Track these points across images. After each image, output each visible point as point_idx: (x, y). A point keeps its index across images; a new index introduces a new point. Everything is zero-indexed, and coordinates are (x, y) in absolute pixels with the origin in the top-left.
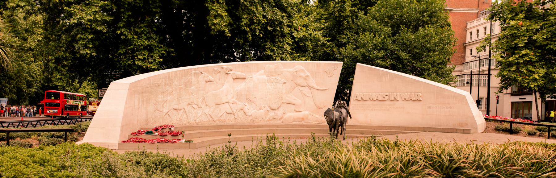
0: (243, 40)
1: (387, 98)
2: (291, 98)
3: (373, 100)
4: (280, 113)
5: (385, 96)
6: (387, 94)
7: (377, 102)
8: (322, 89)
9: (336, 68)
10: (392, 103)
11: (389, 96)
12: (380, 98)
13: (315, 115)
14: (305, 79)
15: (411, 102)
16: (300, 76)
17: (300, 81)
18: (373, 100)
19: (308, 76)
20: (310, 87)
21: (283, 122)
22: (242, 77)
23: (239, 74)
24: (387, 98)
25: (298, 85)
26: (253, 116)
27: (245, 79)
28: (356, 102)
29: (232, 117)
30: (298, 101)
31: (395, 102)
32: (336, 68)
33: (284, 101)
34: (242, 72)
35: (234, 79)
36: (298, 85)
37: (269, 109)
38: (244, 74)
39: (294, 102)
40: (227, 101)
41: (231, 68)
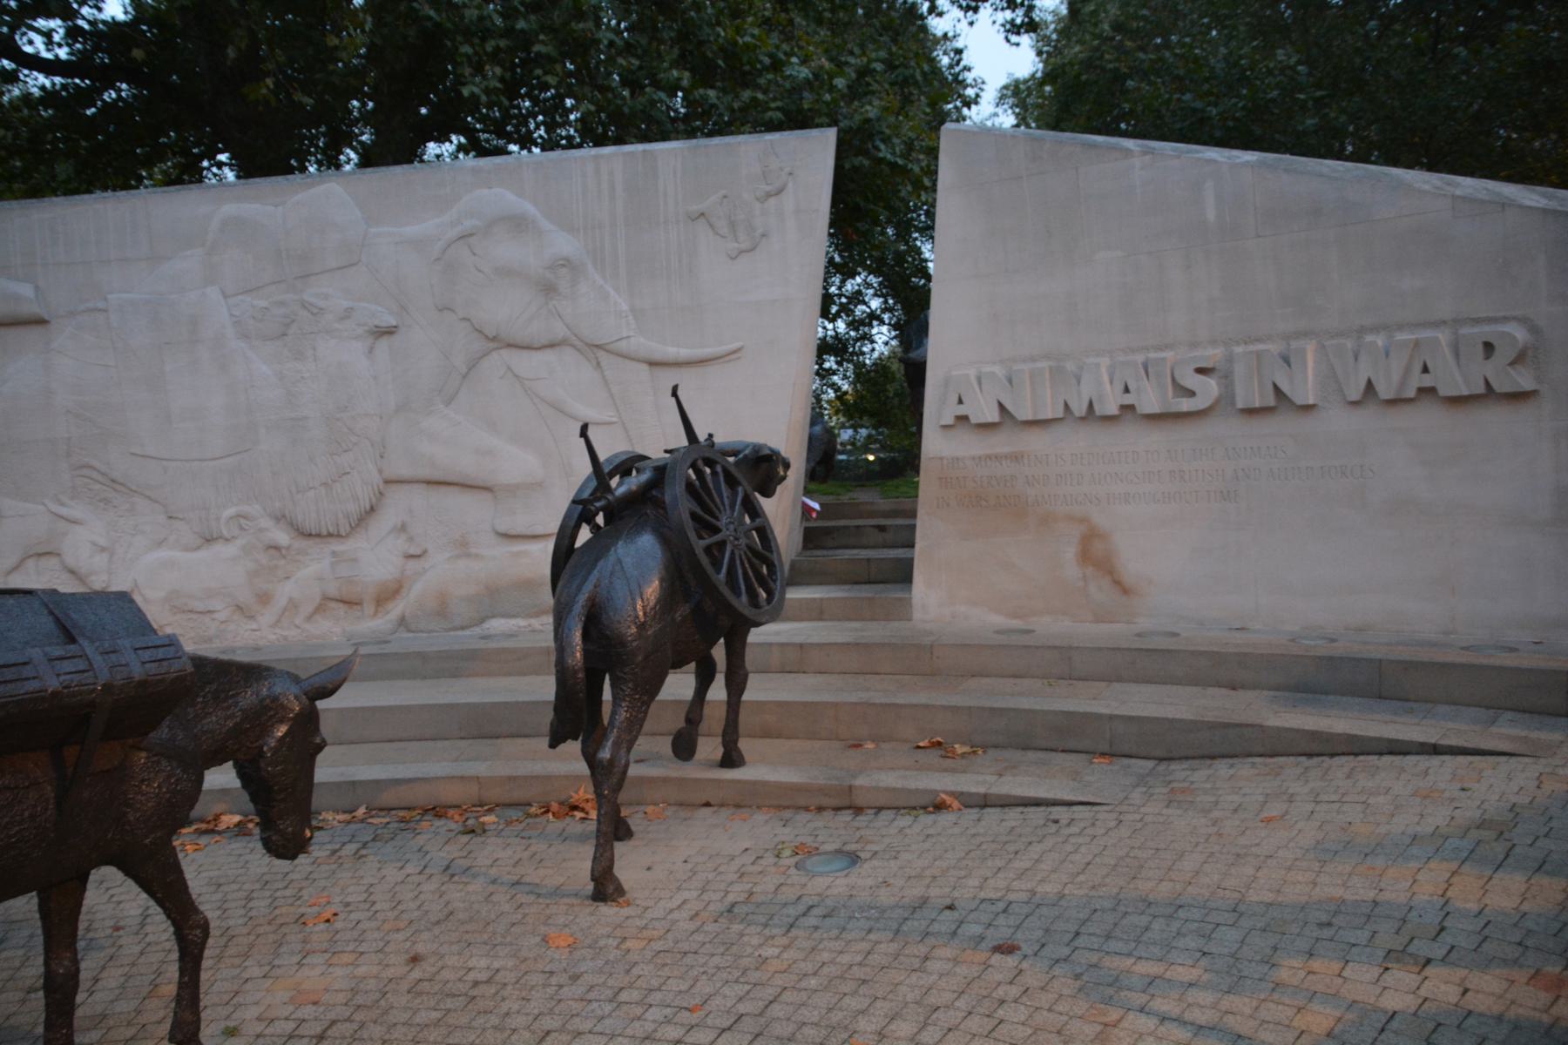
3: (319, 535)
4: (375, 557)
5: (1191, 380)
6: (1211, 355)
7: (1135, 438)
8: (684, 353)
11: (1227, 379)
12: (1150, 400)
14: (548, 289)
15: (1428, 417)
17: (507, 308)
18: (319, 535)
19: (566, 263)
20: (594, 349)
24: (1208, 389)
25: (501, 342)
27: (41, 322)
28: (965, 446)
31: (1281, 426)
36: (501, 342)
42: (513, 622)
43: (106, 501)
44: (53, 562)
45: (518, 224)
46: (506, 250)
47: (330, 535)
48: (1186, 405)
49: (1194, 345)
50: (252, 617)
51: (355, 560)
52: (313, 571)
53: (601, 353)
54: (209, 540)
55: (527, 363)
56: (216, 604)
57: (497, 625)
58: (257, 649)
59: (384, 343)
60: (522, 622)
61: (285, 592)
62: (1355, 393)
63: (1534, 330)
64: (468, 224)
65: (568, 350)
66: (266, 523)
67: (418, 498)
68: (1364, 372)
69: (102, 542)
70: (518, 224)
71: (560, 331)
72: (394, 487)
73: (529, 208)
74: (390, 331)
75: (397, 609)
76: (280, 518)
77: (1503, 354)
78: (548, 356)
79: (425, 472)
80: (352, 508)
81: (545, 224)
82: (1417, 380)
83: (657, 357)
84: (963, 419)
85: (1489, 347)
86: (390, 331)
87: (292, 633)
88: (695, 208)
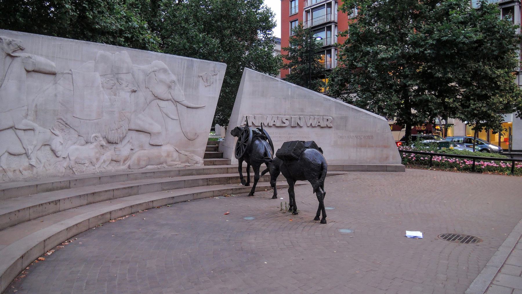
0: (17, 12)
1: (287, 123)
2: (143, 121)
4: (124, 150)
5: (285, 121)
6: (288, 117)
8: (194, 106)
9: (218, 70)
10: (295, 129)
12: (278, 124)
13: (183, 152)
14: (170, 87)
15: (318, 130)
16: (162, 81)
17: (161, 90)
18: (113, 143)
19: (174, 82)
20: (176, 102)
21: (129, 167)
22: (48, 69)
23: (42, 60)
26: (73, 158)
29: (24, 162)
30: (156, 128)
31: (297, 130)
32: (218, 70)
33: (133, 127)
34: (47, 57)
35: (28, 71)
37: (104, 143)
38: (53, 64)
39: (147, 127)
40: (10, 124)
41: (23, 45)
42: (154, 166)
43: (63, 130)
44: (48, 148)
45: (165, 71)
46: (162, 76)
47: (115, 143)
48: (284, 125)
49: (285, 115)
50: (94, 165)
51: (120, 150)
52: (108, 154)
53: (178, 103)
54: (87, 143)
55: (162, 104)
56: (86, 162)
57: (149, 167)
58: (94, 174)
59: (133, 93)
60: (156, 166)
61: (104, 157)
62: (309, 125)
63: (333, 118)
64: (155, 68)
65: (170, 102)
66: (101, 139)
67: (134, 134)
68: (311, 121)
69: (62, 142)
70: (165, 71)
71: (170, 97)
72: (130, 131)
73: (166, 66)
74: (135, 92)
75: (128, 163)
76: (104, 138)
77: (329, 121)
78: (166, 102)
79: (138, 128)
80: (121, 136)
81: (170, 72)
82: (318, 124)
83: (189, 106)
84: (274, 125)
85: (327, 120)
86: (135, 92)
87: (103, 170)
88: (200, 75)
